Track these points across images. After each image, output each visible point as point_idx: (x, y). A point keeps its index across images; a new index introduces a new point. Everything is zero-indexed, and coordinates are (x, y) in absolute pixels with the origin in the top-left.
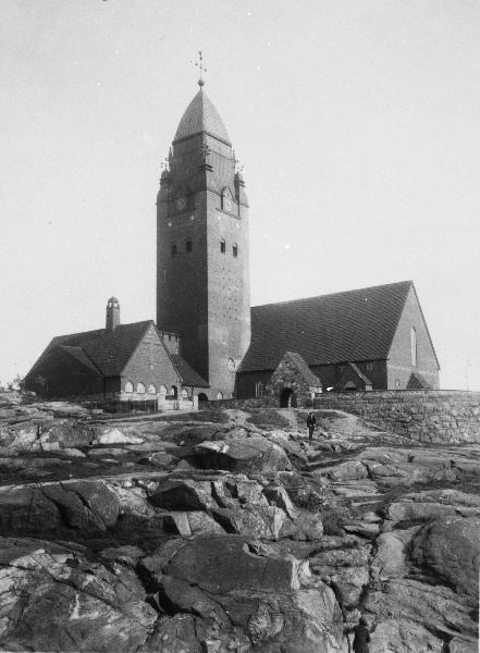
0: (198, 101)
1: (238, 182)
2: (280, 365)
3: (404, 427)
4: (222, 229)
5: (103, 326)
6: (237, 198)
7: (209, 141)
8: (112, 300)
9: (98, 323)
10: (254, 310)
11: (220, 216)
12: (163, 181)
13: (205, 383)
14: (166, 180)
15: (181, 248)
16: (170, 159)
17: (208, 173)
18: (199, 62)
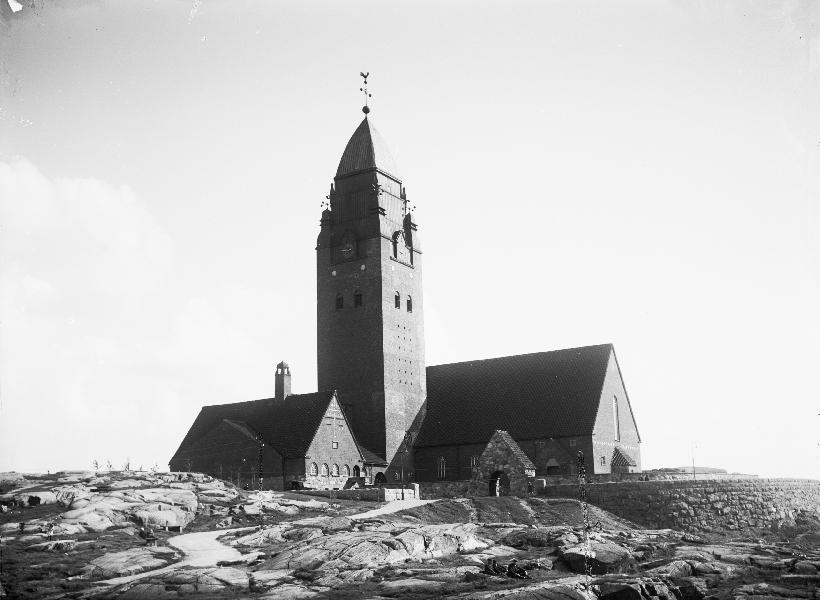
0: (364, 128)
1: (408, 225)
2: (490, 445)
3: (642, 515)
4: (397, 281)
5: (272, 395)
6: (409, 242)
7: (381, 180)
8: (281, 366)
9: (268, 392)
10: (430, 370)
11: (394, 266)
12: (324, 222)
13: (380, 461)
14: (327, 220)
15: (349, 301)
16: (333, 196)
17: (381, 216)
18: (363, 86)
